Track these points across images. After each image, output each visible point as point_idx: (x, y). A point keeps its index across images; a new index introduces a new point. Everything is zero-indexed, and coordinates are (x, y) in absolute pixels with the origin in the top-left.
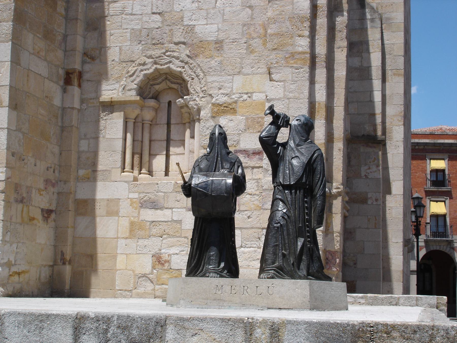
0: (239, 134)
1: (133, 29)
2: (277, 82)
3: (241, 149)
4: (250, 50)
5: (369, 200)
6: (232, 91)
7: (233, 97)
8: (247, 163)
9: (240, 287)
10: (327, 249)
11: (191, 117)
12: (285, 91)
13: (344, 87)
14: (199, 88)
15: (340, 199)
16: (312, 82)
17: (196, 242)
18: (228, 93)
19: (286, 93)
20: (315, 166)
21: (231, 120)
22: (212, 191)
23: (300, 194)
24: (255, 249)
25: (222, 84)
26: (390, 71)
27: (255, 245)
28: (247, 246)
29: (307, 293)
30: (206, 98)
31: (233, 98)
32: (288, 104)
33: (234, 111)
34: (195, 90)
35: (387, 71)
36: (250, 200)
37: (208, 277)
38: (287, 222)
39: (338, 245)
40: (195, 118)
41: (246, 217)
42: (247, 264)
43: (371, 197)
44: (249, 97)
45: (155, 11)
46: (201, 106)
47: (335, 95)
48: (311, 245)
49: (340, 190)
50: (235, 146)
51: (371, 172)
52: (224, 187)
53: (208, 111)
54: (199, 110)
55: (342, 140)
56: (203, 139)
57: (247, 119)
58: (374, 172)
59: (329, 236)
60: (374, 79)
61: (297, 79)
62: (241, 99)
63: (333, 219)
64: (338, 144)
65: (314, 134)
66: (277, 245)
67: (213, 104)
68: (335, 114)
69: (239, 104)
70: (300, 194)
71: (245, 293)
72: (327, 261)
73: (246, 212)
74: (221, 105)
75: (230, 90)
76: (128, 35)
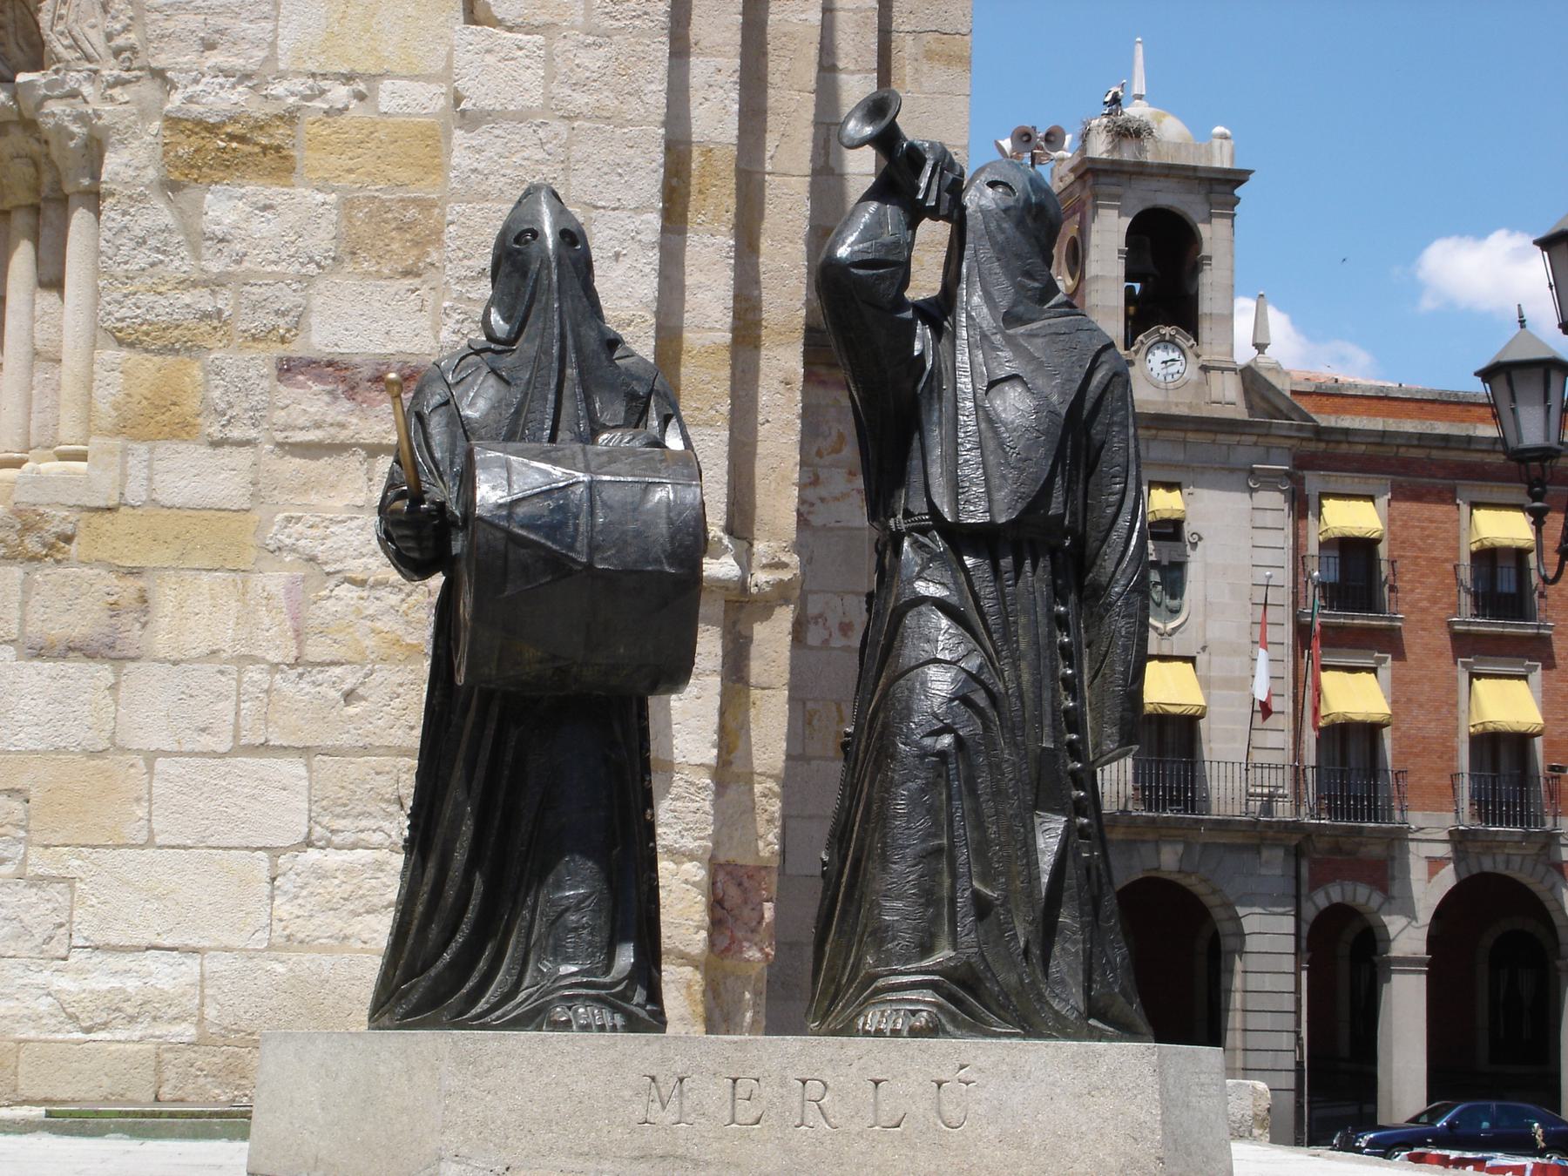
0: (306, 280)
2: (510, 29)
3: (314, 356)
5: (812, 627)
6: (271, 58)
7: (279, 89)
8: (342, 426)
9: (783, 1083)
10: (722, 859)
11: (47, 178)
12: (550, 77)
13: (812, 85)
14: (96, 37)
15: (784, 617)
16: (680, 49)
17: (467, 828)
18: (251, 67)
19: (555, 88)
20: (1097, 430)
21: (266, 208)
22: (593, 548)
23: (1035, 579)
24: (377, 854)
25: (222, 22)
26: (909, 38)
27: (378, 837)
28: (336, 839)
29: (1147, 1111)
30: (133, 88)
31: (277, 98)
32: (567, 146)
33: (278, 163)
34: (76, 45)
35: (894, 36)
36: (358, 611)
37: (566, 1026)
38: (986, 728)
39: (771, 837)
40: (68, 188)
41: (335, 694)
42: (333, 931)
43: (820, 615)
44: (361, 97)
46: (107, 128)
47: (771, 119)
48: (1091, 852)
49: (786, 575)
50: (283, 340)
51: (822, 500)
52: (663, 527)
53: (143, 156)
54: (95, 149)
55: (799, 336)
56: (117, 296)
57: (347, 205)
58: (836, 499)
59: (732, 793)
60: (845, 70)
61: (608, 23)
62: (317, 104)
63: (753, 712)
64: (779, 352)
65: (682, 301)
66: (938, 851)
67: (173, 122)
68: (769, 209)
69: (308, 127)
70: (1035, 579)
71: (810, 1120)
72: (720, 913)
73: (338, 670)
74: (213, 129)
75: (260, 54)
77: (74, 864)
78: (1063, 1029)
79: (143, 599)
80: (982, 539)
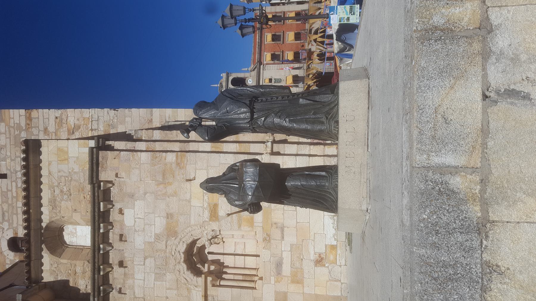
1: (155, 280)
4: (175, 194)
6: (201, 207)
12: (202, 169)
22: (254, 181)
45: (142, 263)
74: (211, 215)
76: (158, 283)
77: (312, 233)
78: (337, 99)
79: (275, 224)
80: (252, 113)
